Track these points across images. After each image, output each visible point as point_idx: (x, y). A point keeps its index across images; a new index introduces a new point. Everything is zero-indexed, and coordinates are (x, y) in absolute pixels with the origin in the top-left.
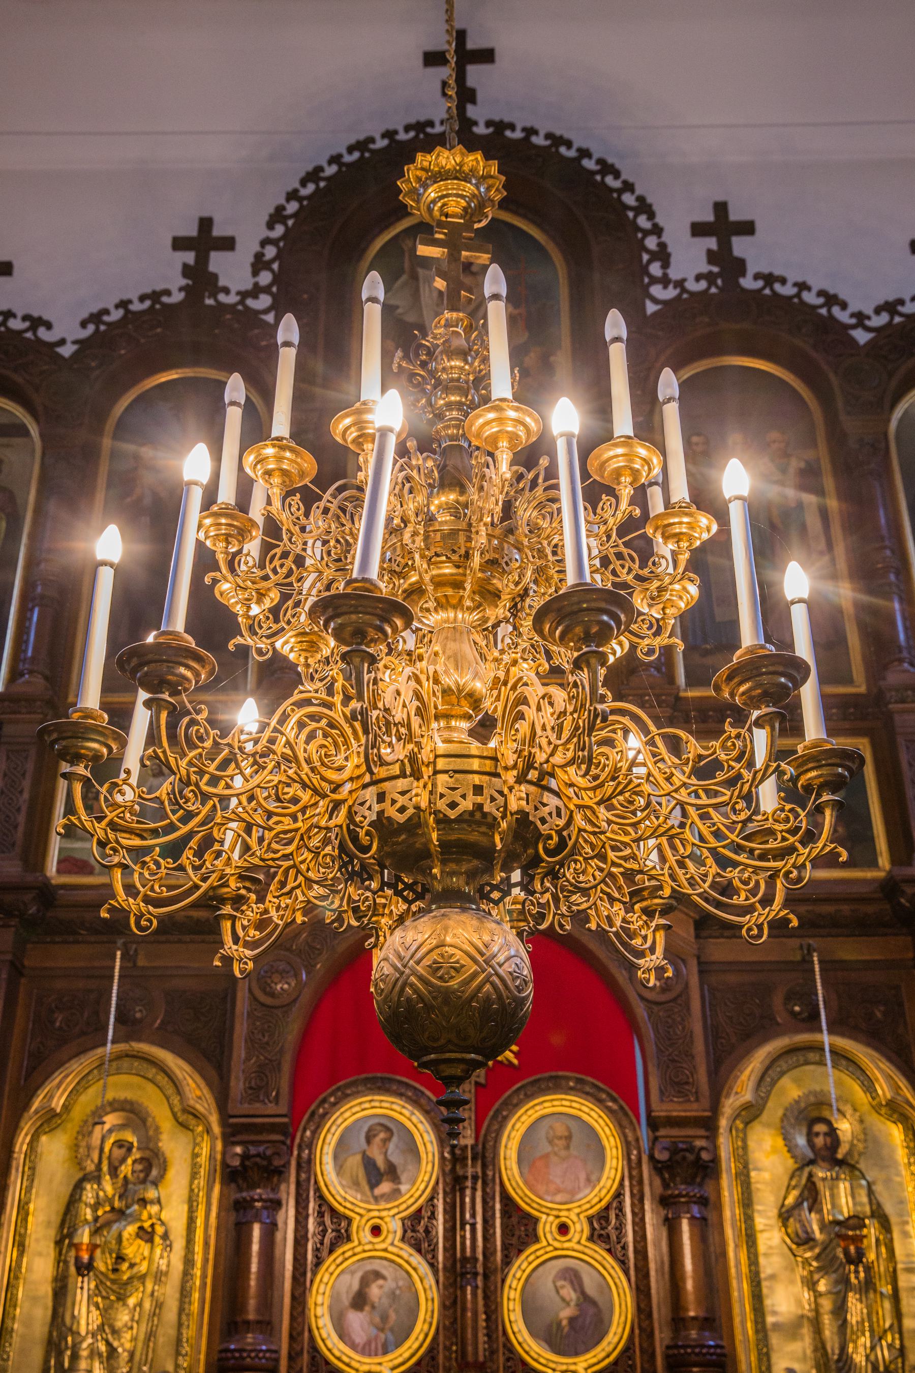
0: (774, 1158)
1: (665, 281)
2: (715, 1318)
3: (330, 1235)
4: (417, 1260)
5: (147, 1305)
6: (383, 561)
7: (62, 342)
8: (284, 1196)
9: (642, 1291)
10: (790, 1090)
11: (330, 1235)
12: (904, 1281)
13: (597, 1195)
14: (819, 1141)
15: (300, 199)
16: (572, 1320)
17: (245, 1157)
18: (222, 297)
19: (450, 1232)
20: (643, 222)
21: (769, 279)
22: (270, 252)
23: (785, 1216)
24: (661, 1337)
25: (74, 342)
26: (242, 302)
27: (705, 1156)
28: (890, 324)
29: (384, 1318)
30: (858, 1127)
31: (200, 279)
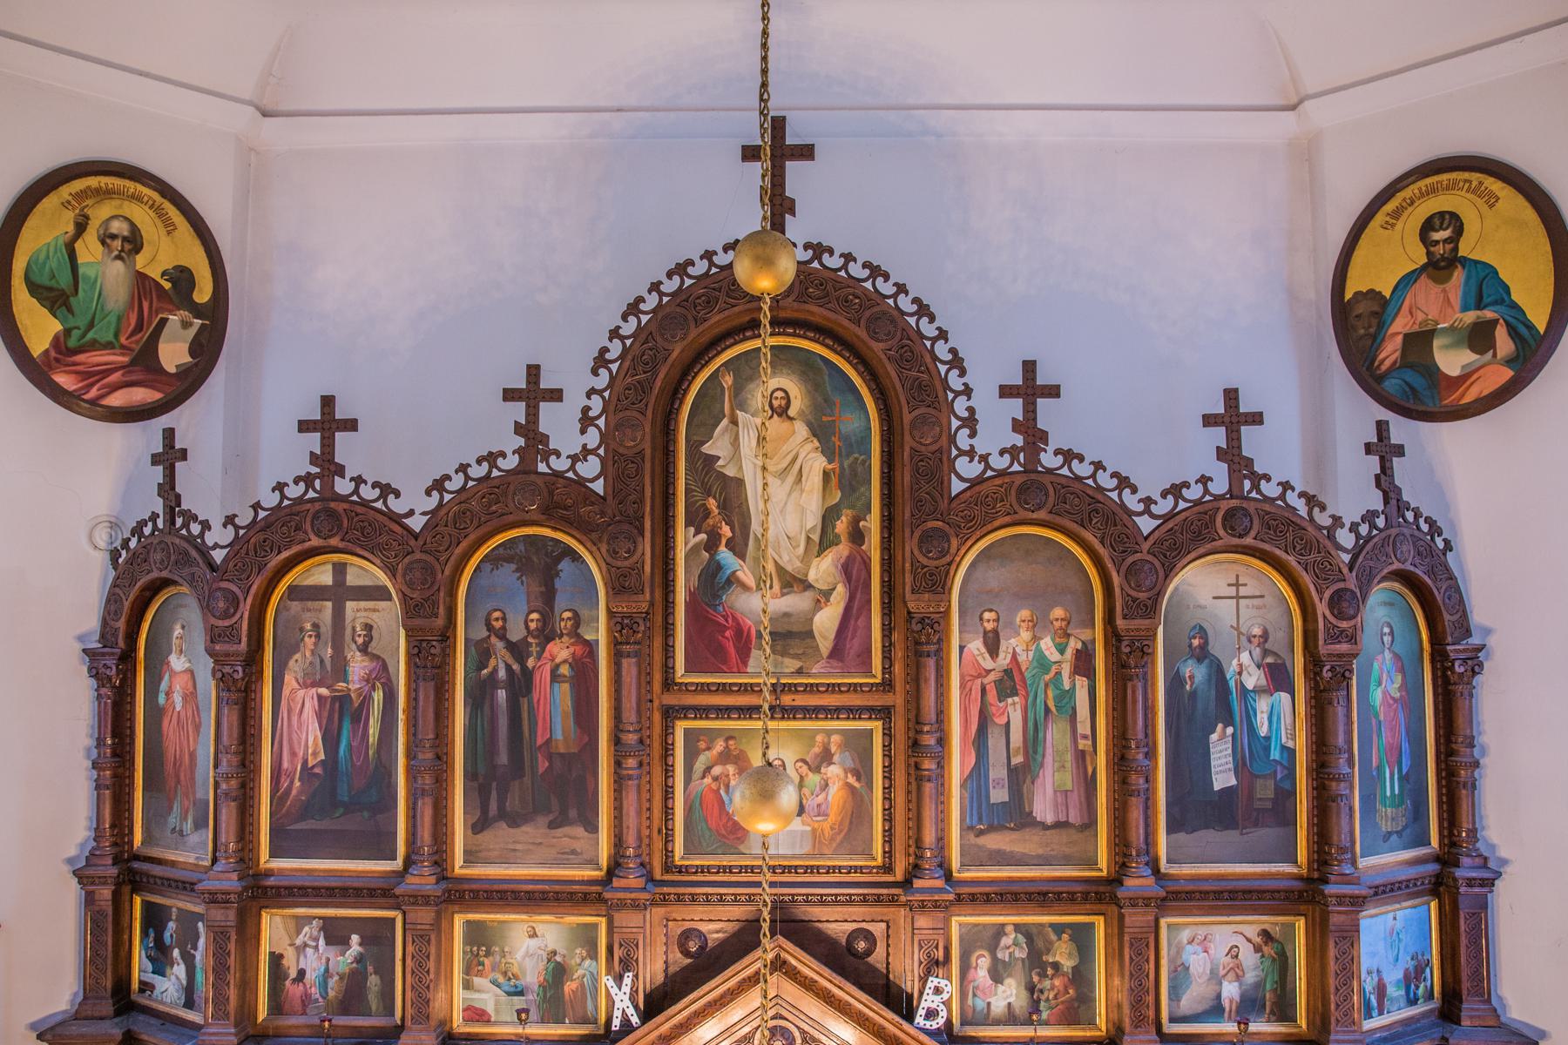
1: (971, 453)
7: (411, 513)
21: (1069, 456)
22: (596, 404)
25: (424, 514)
26: (573, 468)
31: (533, 439)
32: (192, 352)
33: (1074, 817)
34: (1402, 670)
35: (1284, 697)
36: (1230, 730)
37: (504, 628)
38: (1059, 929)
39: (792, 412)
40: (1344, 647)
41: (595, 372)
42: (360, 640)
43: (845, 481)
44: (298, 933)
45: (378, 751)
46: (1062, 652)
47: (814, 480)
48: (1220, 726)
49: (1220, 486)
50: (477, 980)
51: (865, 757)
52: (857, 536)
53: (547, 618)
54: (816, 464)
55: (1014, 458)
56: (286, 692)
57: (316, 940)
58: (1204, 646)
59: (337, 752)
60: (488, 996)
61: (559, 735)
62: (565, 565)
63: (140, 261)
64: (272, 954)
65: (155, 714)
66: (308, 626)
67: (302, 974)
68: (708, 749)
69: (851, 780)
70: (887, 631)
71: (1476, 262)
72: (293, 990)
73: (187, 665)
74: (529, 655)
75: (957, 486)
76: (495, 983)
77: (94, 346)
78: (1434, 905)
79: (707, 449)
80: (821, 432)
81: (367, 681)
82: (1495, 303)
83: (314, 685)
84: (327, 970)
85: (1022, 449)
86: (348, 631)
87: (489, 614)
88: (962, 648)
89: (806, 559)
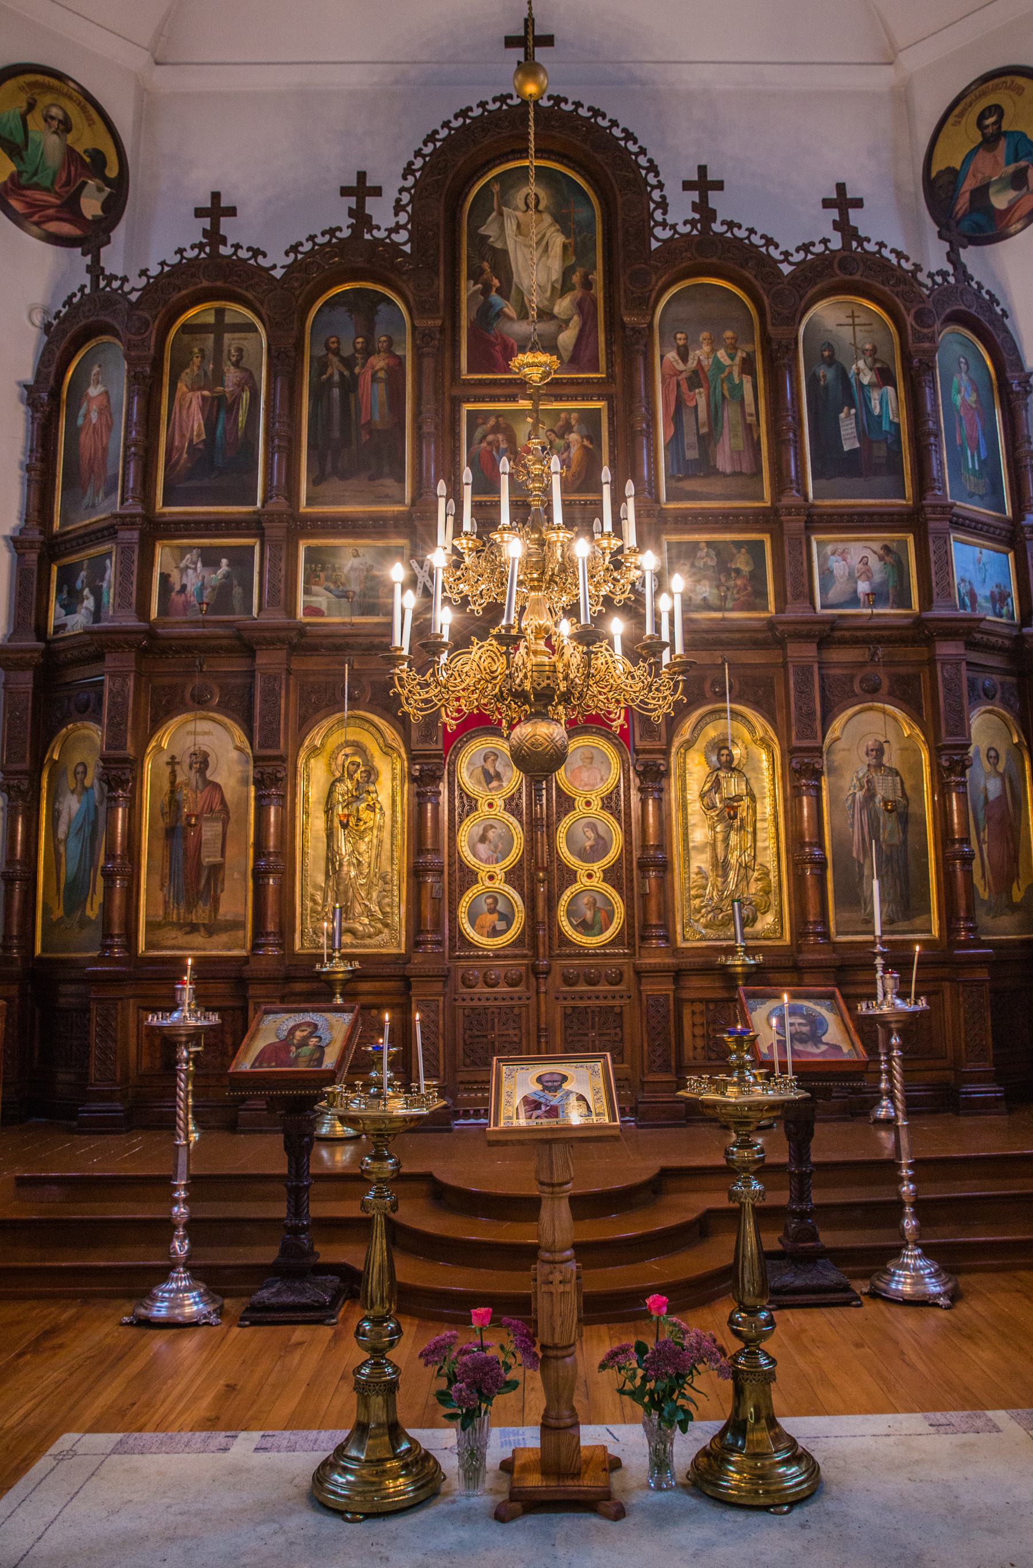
0: (699, 768)
1: (664, 224)
2: (663, 844)
3: (467, 807)
4: (512, 819)
5: (375, 841)
6: (465, 1043)
7: (274, 267)
8: (441, 788)
9: (627, 833)
10: (711, 732)
11: (467, 807)
12: (759, 825)
13: (605, 788)
14: (723, 759)
15: (424, 156)
16: (591, 847)
17: (421, 771)
18: (375, 232)
19: (529, 805)
20: (651, 179)
21: (731, 225)
22: (406, 198)
23: (702, 796)
24: (636, 854)
26: (389, 236)
27: (662, 768)
28: (804, 261)
29: (496, 847)
30: (744, 752)
31: (361, 219)
32: (103, 209)
33: (746, 468)
34: (976, 390)
35: (890, 389)
36: (853, 411)
37: (338, 348)
38: (738, 544)
39: (541, 207)
40: (926, 345)
41: (405, 178)
42: (234, 359)
43: (577, 252)
44: (182, 559)
45: (245, 433)
46: (732, 359)
47: (557, 249)
48: (846, 409)
49: (836, 244)
50: (315, 588)
51: (594, 437)
52: (587, 285)
53: (369, 341)
54: (558, 240)
55: (694, 226)
56: (178, 395)
57: (196, 563)
58: (832, 356)
59: (215, 434)
60: (322, 599)
61: (377, 417)
62: (382, 307)
63: (70, 138)
64: (162, 574)
65: (73, 433)
66: (196, 350)
67: (184, 587)
68: (484, 423)
69: (586, 443)
70: (609, 344)
71: (1013, 133)
72: (177, 599)
73: (106, 387)
74: (356, 365)
75: (655, 245)
76: (327, 589)
77: (36, 187)
78: (1011, 555)
79: (482, 230)
80: (562, 221)
81: (238, 385)
82: (1027, 155)
83: (200, 389)
84: (203, 584)
85: (699, 221)
86: (225, 353)
87: (327, 340)
88: (662, 357)
89: (552, 300)
